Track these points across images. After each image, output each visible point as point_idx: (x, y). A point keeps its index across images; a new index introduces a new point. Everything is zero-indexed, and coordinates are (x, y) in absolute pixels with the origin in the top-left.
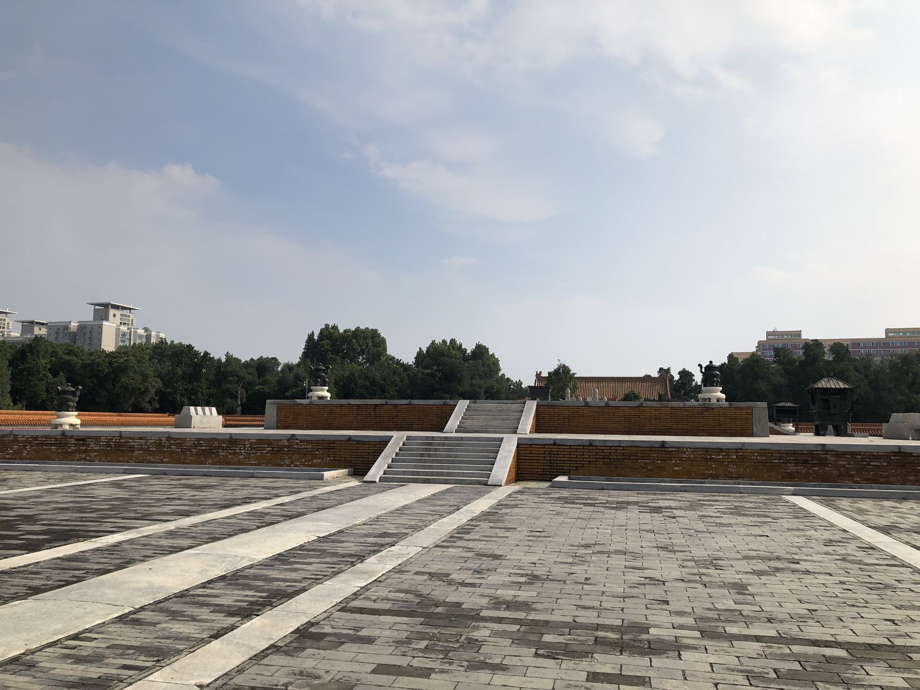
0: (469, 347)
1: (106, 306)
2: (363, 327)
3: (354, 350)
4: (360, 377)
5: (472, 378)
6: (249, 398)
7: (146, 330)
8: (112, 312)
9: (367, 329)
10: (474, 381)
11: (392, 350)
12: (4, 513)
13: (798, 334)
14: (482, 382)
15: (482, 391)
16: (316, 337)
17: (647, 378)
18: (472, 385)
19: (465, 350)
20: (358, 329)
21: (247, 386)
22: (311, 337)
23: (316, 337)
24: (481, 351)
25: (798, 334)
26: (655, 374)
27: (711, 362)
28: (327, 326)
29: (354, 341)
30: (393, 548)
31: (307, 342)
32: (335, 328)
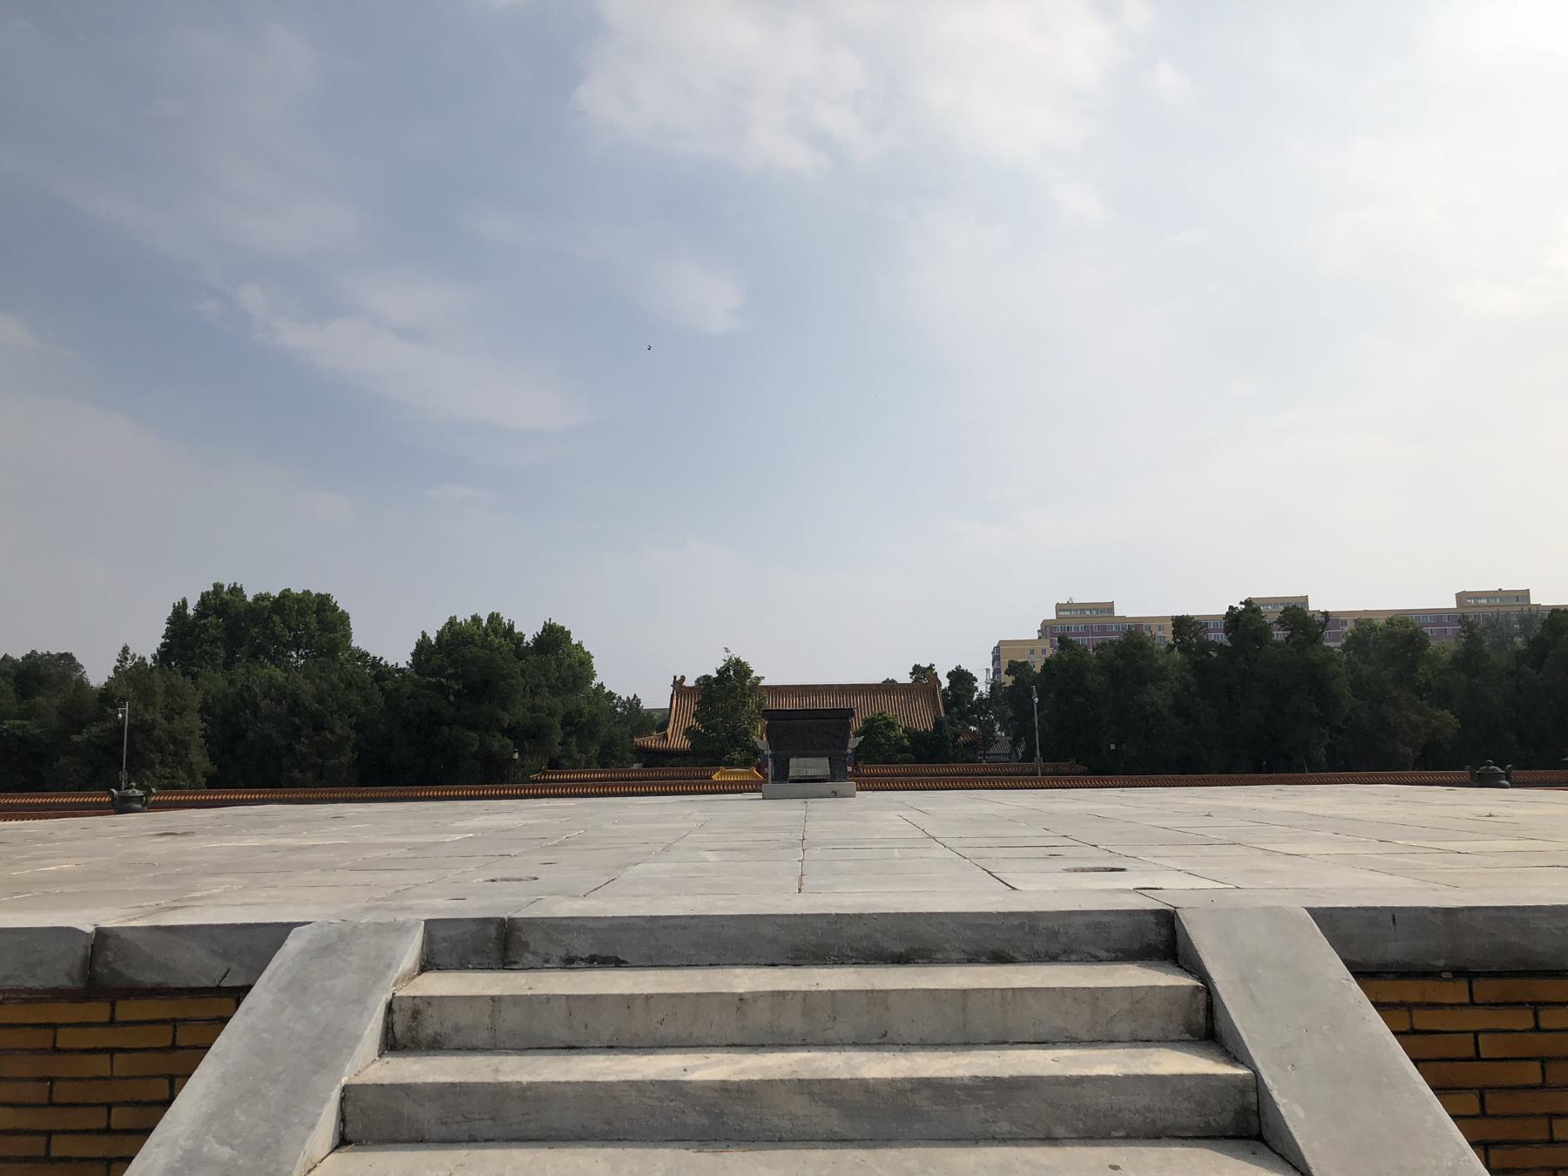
0: (529, 630)
2: (297, 589)
3: (276, 638)
4: (266, 695)
5: (534, 693)
10: (538, 700)
13: (1109, 607)
14: (556, 701)
15: (556, 722)
16: (190, 612)
17: (889, 687)
18: (533, 709)
19: (521, 637)
20: (286, 594)
23: (190, 612)
24: (553, 638)
25: (1109, 607)
26: (904, 678)
28: (218, 587)
29: (276, 618)
31: (170, 621)
32: (236, 591)
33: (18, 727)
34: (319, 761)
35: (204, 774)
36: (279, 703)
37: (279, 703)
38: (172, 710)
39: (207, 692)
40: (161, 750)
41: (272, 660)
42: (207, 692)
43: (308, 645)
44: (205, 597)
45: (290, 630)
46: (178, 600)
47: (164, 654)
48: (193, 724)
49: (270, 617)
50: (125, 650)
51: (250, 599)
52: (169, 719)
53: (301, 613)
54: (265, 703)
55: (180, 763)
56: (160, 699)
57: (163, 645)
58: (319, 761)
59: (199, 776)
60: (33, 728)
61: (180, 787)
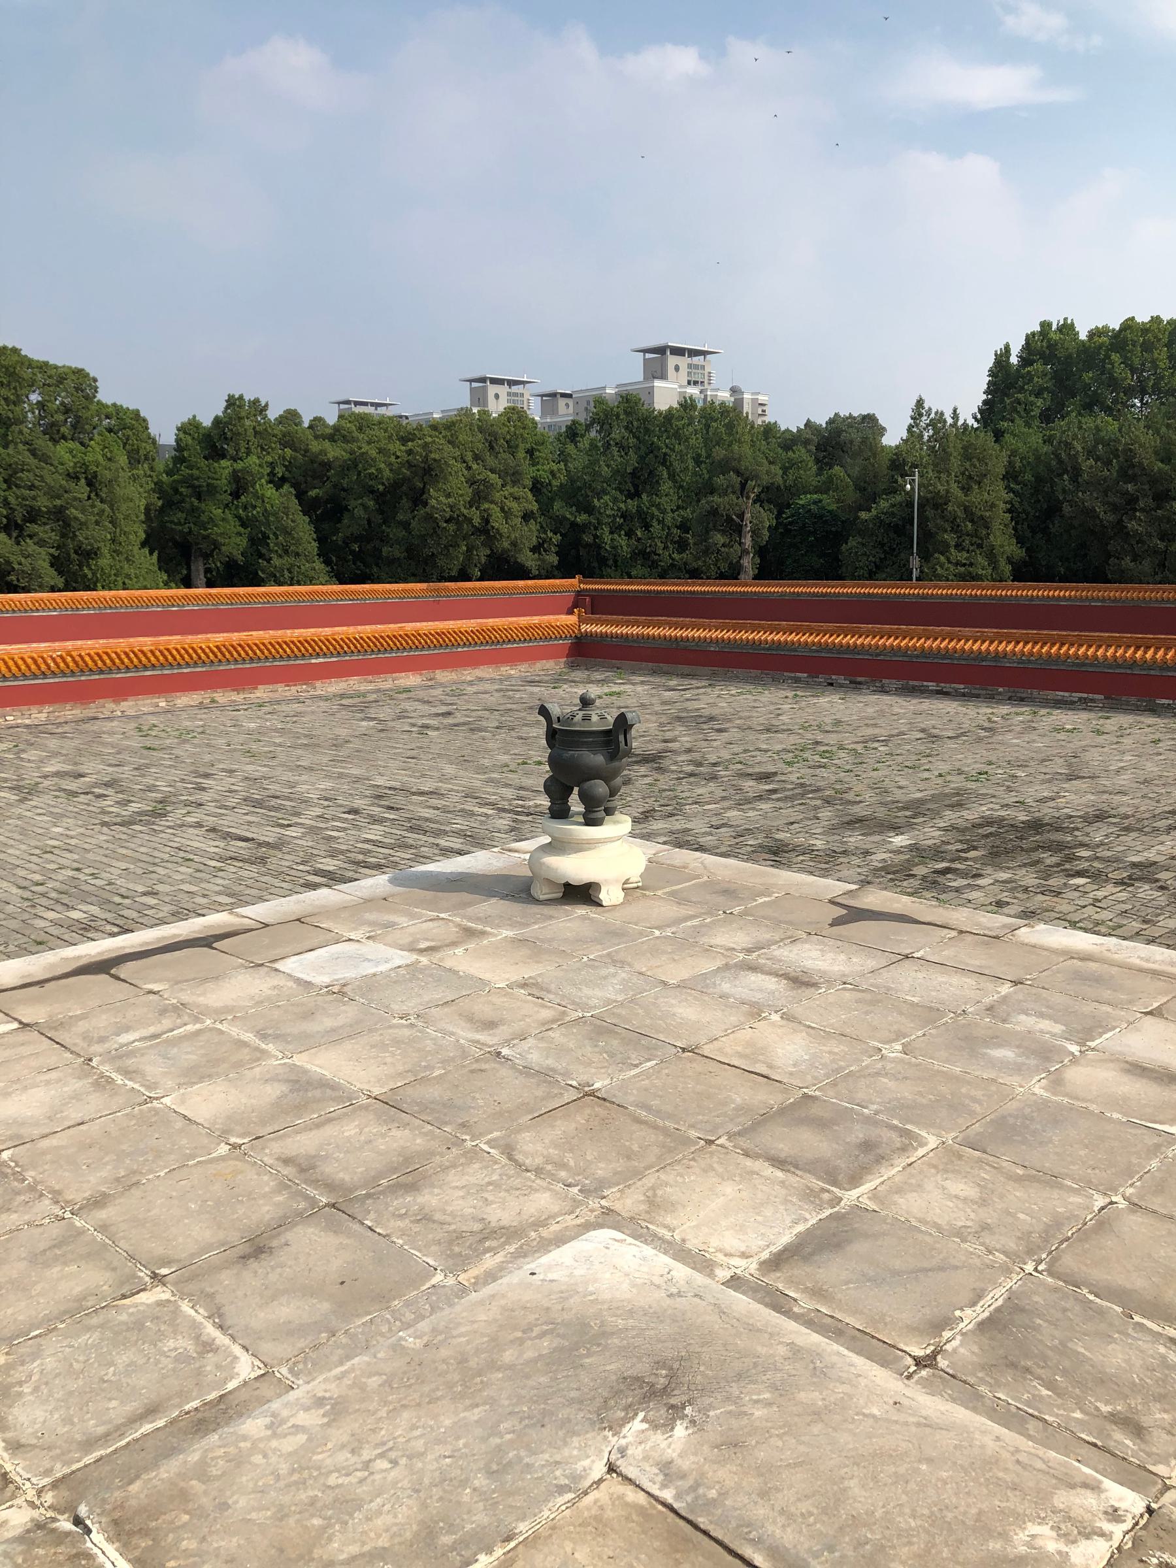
1: (661, 350)
2: (1143, 318)
3: (1113, 383)
4: (1090, 453)
6: (781, 530)
7: (734, 390)
8: (672, 360)
9: (1156, 320)
11: (153, 430)
12: (1172, 1332)
16: (1014, 360)
20: (1129, 325)
21: (772, 496)
22: (1002, 359)
23: (1014, 360)
27: (194, 417)
28: (1045, 325)
29: (1115, 357)
30: (460, 858)
31: (992, 373)
32: (1067, 328)
33: (815, 503)
34: (1161, 545)
35: (1009, 560)
36: (1108, 463)
37: (1108, 463)
38: (970, 477)
39: (1014, 453)
40: (956, 529)
41: (1108, 410)
42: (1014, 453)
43: (1156, 389)
44: (1030, 338)
45: (1133, 370)
46: (999, 347)
47: (988, 413)
48: (995, 497)
49: (1108, 357)
50: (920, 403)
51: (1083, 336)
52: (966, 489)
53: (1147, 347)
54: (1087, 464)
55: (980, 546)
56: (955, 463)
57: (985, 402)
58: (1161, 545)
59: (1002, 562)
60: (829, 502)
61: (939, 578)
